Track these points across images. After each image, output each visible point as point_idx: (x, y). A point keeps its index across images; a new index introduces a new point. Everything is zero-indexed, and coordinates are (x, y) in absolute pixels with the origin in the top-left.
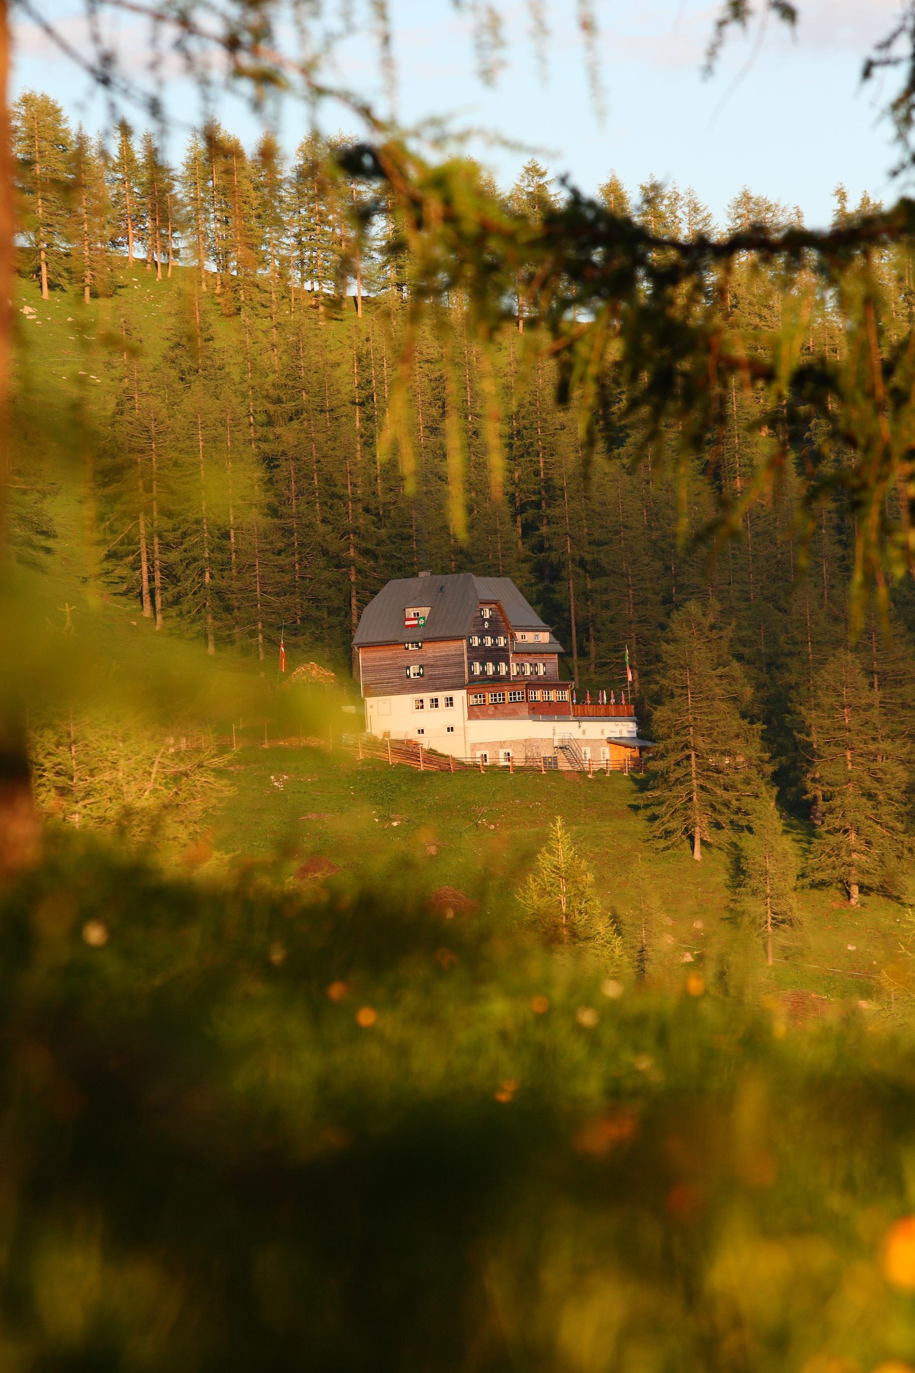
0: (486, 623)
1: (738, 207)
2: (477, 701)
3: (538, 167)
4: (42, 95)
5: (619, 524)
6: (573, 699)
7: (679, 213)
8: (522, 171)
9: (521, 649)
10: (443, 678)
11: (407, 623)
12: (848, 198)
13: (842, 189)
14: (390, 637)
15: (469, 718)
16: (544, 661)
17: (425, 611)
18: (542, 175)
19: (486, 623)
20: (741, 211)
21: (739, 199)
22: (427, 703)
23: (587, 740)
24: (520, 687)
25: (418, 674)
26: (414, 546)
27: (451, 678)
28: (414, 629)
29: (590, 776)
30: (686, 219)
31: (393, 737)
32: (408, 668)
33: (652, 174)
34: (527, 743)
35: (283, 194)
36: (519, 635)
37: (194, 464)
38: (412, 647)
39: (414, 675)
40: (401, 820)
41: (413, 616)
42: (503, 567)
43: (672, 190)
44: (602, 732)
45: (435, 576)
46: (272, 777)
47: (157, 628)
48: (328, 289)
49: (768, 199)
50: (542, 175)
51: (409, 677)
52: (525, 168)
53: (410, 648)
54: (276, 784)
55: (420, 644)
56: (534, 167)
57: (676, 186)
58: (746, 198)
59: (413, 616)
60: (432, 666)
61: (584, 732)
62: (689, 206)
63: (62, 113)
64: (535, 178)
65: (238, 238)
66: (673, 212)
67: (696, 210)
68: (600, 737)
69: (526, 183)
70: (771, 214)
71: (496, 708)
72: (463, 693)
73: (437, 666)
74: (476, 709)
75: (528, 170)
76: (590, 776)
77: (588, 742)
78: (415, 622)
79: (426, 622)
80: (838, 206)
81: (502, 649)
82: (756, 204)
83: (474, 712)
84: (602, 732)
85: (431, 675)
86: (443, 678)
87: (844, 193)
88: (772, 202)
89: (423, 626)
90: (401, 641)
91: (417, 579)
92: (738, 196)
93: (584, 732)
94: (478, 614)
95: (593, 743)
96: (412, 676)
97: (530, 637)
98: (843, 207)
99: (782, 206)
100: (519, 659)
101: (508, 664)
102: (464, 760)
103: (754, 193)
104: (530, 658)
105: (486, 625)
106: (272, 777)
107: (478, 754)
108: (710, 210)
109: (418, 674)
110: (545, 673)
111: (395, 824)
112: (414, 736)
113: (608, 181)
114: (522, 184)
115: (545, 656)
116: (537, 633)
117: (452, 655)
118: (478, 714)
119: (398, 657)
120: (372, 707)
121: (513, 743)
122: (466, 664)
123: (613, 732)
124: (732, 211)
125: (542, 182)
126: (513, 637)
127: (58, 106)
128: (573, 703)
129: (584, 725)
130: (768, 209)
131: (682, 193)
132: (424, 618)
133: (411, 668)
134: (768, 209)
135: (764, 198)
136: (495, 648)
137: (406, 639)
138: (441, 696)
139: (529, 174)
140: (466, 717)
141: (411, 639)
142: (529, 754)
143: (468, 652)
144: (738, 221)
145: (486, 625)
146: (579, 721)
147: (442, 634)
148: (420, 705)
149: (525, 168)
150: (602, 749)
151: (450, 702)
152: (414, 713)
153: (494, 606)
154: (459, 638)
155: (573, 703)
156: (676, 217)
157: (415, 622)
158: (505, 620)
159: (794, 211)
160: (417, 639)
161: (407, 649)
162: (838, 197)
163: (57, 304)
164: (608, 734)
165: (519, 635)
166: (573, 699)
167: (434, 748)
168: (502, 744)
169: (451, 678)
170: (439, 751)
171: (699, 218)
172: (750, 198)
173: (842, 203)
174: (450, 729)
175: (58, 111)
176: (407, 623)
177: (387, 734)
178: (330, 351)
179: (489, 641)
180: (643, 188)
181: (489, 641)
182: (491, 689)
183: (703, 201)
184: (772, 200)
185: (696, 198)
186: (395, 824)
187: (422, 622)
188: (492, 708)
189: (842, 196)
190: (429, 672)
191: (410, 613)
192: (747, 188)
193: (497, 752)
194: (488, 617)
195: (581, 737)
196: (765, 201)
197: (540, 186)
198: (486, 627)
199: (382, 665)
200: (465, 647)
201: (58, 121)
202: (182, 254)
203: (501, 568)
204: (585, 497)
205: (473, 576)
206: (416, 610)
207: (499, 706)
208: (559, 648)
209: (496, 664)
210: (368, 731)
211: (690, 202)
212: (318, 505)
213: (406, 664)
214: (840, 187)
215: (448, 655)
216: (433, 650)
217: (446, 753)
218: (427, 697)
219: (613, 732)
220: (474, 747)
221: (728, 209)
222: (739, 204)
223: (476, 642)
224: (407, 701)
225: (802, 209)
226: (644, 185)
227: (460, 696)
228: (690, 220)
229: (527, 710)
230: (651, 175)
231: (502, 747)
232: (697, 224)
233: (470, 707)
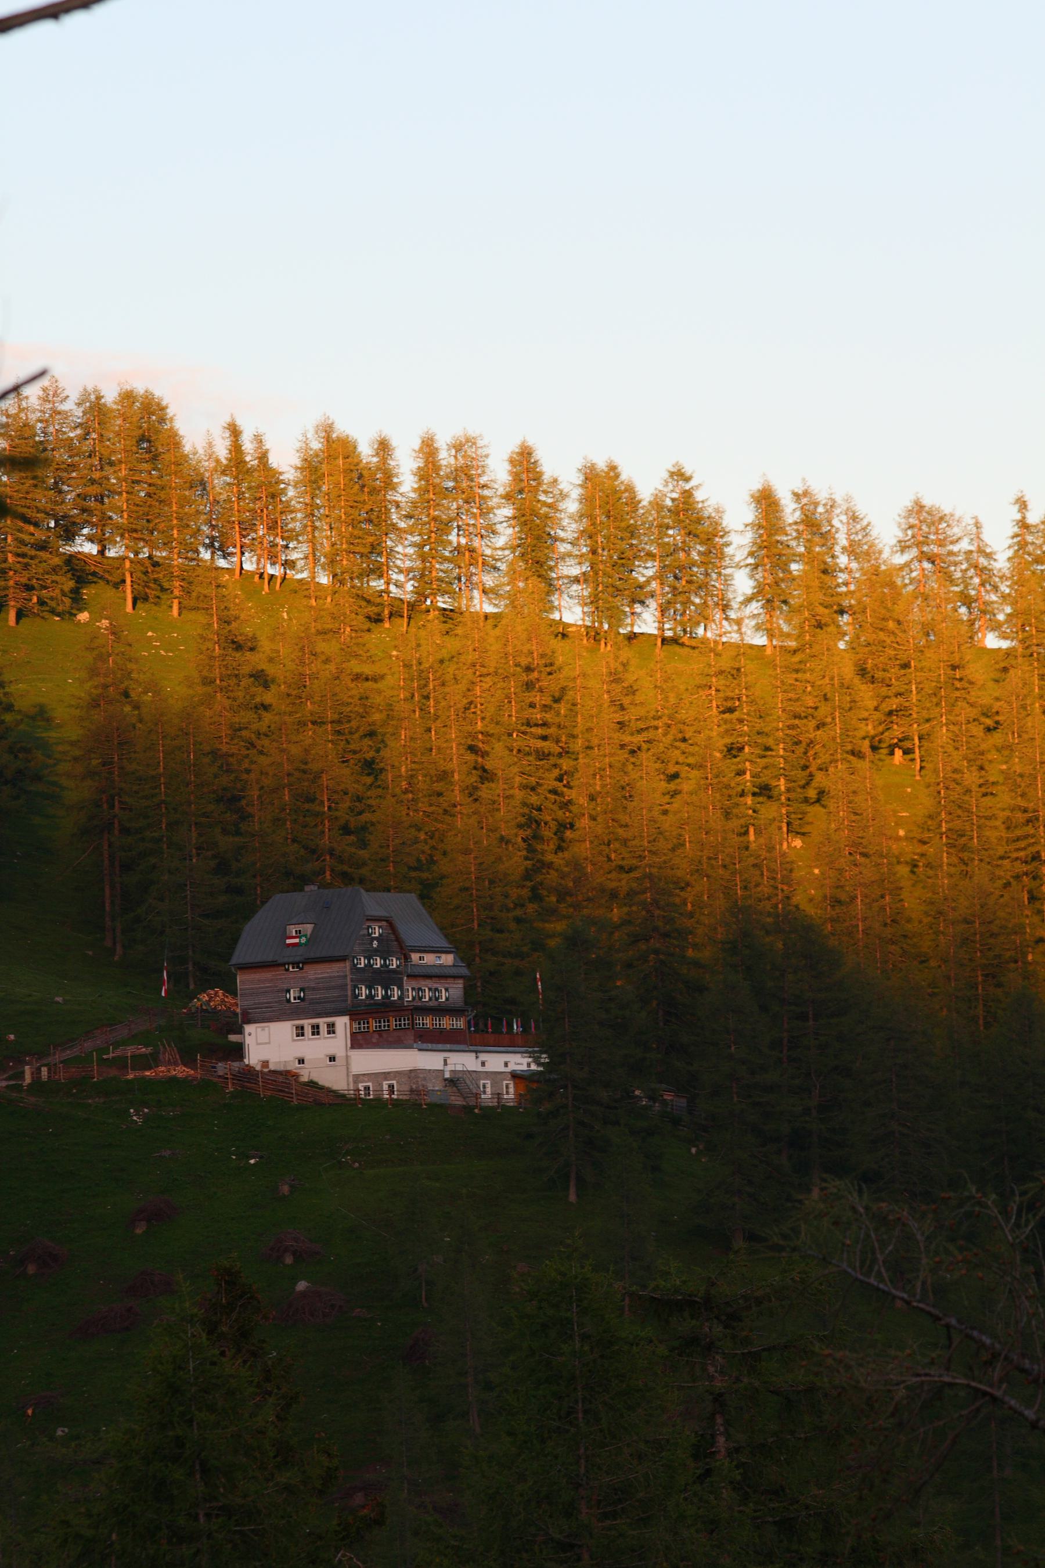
0: (375, 942)
1: (907, 518)
2: (360, 1028)
3: (683, 471)
4: (146, 392)
5: (642, 848)
6: (469, 1028)
7: (835, 522)
8: (666, 475)
9: (416, 971)
10: (325, 1002)
11: (288, 941)
12: (1029, 507)
13: (1022, 497)
14: (269, 957)
15: (352, 1047)
16: (447, 986)
17: (309, 928)
18: (688, 479)
19: (375, 942)
20: (912, 521)
21: (910, 508)
22: (308, 1030)
23: (486, 1072)
24: (407, 1013)
25: (299, 998)
26: (391, 869)
27: (333, 1002)
28: (296, 948)
29: (476, 1111)
30: (843, 529)
31: (272, 1067)
32: (288, 991)
33: (804, 479)
34: (413, 1074)
35: (400, 499)
36: (415, 957)
37: (153, 777)
38: (293, 968)
39: (295, 999)
40: (261, 1157)
41: (294, 934)
42: (477, 890)
43: (828, 497)
44: (506, 1064)
45: (321, 890)
46: (132, 1111)
47: (116, 958)
48: (444, 602)
49: (942, 508)
50: (688, 479)
51: (289, 1001)
52: (669, 471)
53: (291, 970)
54: (135, 1118)
55: (301, 965)
56: (679, 470)
57: (833, 491)
58: (918, 508)
59: (294, 934)
60: (314, 989)
61: (483, 1064)
62: (846, 514)
63: (168, 411)
64: (680, 483)
65: (344, 546)
66: (829, 522)
67: (854, 518)
68: (503, 1069)
69: (671, 487)
70: (945, 525)
71: (380, 1036)
72: (346, 1019)
73: (319, 989)
74: (359, 1037)
75: (672, 474)
76: (476, 1111)
77: (488, 1075)
78: (296, 941)
79: (308, 940)
80: (1018, 517)
81: (394, 971)
82: (929, 513)
83: (358, 1041)
84: (506, 1064)
85: (312, 999)
86: (317, 1003)
87: (1025, 502)
88: (947, 512)
89: (305, 944)
90: (281, 961)
91: (303, 893)
92: (909, 504)
93: (483, 1064)
94: (365, 932)
95: (494, 1075)
96: (293, 1001)
97: (429, 959)
98: (1024, 518)
99: (956, 517)
100: (415, 984)
101: (400, 987)
102: (346, 1092)
103: (927, 502)
104: (429, 983)
105: (375, 944)
106: (132, 1111)
107: (361, 1086)
108: (401, 463)
109: (299, 998)
110: (447, 999)
111: (252, 1161)
112: (294, 1066)
113: (760, 487)
114: (666, 490)
115: (450, 981)
116: (439, 955)
117: (334, 977)
118: (361, 1042)
119: (277, 979)
120: (250, 1034)
121: (397, 1074)
122: (349, 987)
123: (518, 1064)
124: (903, 520)
125: (687, 487)
126: (407, 958)
127: (164, 403)
128: (470, 1031)
129: (483, 1057)
130: (941, 519)
131: (839, 499)
132: (305, 936)
133: (292, 991)
134: (941, 519)
135: (937, 506)
136: (385, 969)
137: (286, 960)
138: (322, 1022)
139: (673, 479)
140: (349, 1045)
141: (291, 960)
142: (414, 1087)
143: (352, 973)
144: (910, 532)
145: (375, 944)
146: (476, 1052)
147: (324, 954)
148: (300, 1031)
149: (669, 471)
150: (505, 1082)
151: (331, 1029)
152: (294, 1040)
153: (384, 923)
154: (342, 959)
155: (470, 1031)
156: (832, 526)
157: (296, 941)
158: (398, 940)
159: (972, 522)
160: (297, 959)
161: (288, 970)
162: (1017, 507)
163: (142, 618)
164: (512, 1067)
165: (415, 957)
166: (469, 1028)
167: (316, 1080)
168: (386, 1075)
169: (333, 1002)
170: (320, 1083)
171: (858, 527)
172: (922, 507)
173: (1022, 513)
174: (332, 1059)
175: (163, 409)
176: (288, 941)
177: (265, 1064)
178: (373, 662)
179: (378, 963)
180: (580, 470)
181: (378, 963)
182: (374, 1015)
183: (862, 509)
184: (946, 509)
185: (855, 505)
186: (252, 1161)
187: (303, 940)
188: (376, 1036)
189: (1022, 505)
190: (310, 995)
191: (292, 930)
192: (919, 495)
193: (381, 1085)
194: (377, 935)
195: (480, 1069)
196: (938, 510)
197: (686, 491)
198: (375, 946)
199: (260, 988)
200: (348, 968)
201: (162, 420)
202: (300, 564)
203: (474, 891)
204: (613, 820)
205: (362, 891)
206: (299, 927)
207: (385, 1035)
208: (464, 971)
209: (386, 988)
210: (246, 1061)
211: (848, 509)
212: (288, 823)
213: (285, 986)
214: (1020, 495)
215: (330, 977)
216: (315, 973)
217: (327, 1084)
218: (307, 1023)
219: (518, 1064)
220: (357, 1078)
221: (898, 519)
222: (910, 512)
223: (363, 963)
224: (283, 1030)
225: (981, 519)
226: (796, 490)
227: (342, 1023)
228: (849, 530)
229: (412, 1038)
230: (804, 479)
231: (386, 1079)
232: (857, 533)
233: (353, 1034)
